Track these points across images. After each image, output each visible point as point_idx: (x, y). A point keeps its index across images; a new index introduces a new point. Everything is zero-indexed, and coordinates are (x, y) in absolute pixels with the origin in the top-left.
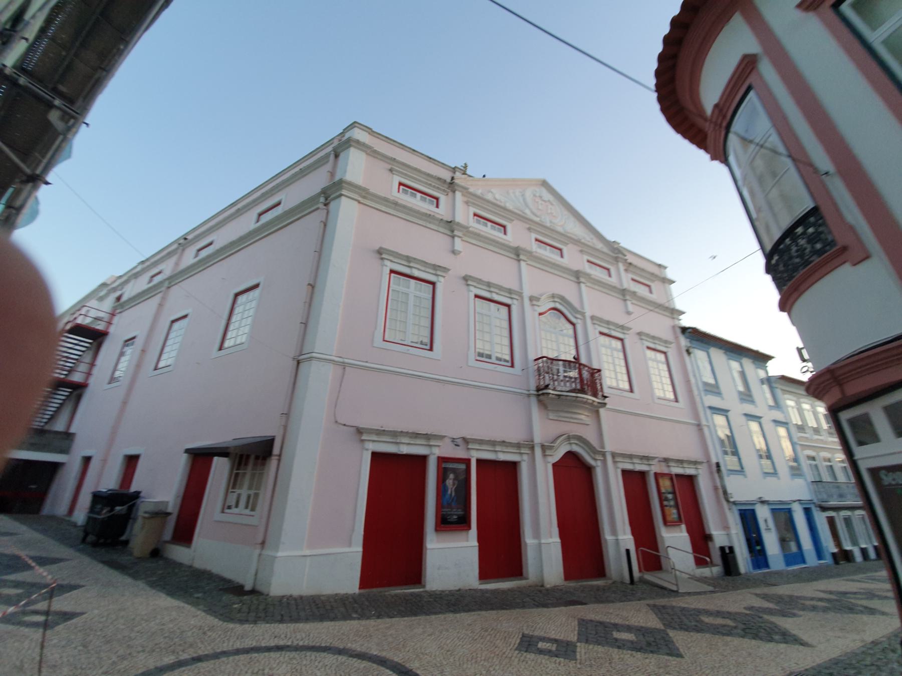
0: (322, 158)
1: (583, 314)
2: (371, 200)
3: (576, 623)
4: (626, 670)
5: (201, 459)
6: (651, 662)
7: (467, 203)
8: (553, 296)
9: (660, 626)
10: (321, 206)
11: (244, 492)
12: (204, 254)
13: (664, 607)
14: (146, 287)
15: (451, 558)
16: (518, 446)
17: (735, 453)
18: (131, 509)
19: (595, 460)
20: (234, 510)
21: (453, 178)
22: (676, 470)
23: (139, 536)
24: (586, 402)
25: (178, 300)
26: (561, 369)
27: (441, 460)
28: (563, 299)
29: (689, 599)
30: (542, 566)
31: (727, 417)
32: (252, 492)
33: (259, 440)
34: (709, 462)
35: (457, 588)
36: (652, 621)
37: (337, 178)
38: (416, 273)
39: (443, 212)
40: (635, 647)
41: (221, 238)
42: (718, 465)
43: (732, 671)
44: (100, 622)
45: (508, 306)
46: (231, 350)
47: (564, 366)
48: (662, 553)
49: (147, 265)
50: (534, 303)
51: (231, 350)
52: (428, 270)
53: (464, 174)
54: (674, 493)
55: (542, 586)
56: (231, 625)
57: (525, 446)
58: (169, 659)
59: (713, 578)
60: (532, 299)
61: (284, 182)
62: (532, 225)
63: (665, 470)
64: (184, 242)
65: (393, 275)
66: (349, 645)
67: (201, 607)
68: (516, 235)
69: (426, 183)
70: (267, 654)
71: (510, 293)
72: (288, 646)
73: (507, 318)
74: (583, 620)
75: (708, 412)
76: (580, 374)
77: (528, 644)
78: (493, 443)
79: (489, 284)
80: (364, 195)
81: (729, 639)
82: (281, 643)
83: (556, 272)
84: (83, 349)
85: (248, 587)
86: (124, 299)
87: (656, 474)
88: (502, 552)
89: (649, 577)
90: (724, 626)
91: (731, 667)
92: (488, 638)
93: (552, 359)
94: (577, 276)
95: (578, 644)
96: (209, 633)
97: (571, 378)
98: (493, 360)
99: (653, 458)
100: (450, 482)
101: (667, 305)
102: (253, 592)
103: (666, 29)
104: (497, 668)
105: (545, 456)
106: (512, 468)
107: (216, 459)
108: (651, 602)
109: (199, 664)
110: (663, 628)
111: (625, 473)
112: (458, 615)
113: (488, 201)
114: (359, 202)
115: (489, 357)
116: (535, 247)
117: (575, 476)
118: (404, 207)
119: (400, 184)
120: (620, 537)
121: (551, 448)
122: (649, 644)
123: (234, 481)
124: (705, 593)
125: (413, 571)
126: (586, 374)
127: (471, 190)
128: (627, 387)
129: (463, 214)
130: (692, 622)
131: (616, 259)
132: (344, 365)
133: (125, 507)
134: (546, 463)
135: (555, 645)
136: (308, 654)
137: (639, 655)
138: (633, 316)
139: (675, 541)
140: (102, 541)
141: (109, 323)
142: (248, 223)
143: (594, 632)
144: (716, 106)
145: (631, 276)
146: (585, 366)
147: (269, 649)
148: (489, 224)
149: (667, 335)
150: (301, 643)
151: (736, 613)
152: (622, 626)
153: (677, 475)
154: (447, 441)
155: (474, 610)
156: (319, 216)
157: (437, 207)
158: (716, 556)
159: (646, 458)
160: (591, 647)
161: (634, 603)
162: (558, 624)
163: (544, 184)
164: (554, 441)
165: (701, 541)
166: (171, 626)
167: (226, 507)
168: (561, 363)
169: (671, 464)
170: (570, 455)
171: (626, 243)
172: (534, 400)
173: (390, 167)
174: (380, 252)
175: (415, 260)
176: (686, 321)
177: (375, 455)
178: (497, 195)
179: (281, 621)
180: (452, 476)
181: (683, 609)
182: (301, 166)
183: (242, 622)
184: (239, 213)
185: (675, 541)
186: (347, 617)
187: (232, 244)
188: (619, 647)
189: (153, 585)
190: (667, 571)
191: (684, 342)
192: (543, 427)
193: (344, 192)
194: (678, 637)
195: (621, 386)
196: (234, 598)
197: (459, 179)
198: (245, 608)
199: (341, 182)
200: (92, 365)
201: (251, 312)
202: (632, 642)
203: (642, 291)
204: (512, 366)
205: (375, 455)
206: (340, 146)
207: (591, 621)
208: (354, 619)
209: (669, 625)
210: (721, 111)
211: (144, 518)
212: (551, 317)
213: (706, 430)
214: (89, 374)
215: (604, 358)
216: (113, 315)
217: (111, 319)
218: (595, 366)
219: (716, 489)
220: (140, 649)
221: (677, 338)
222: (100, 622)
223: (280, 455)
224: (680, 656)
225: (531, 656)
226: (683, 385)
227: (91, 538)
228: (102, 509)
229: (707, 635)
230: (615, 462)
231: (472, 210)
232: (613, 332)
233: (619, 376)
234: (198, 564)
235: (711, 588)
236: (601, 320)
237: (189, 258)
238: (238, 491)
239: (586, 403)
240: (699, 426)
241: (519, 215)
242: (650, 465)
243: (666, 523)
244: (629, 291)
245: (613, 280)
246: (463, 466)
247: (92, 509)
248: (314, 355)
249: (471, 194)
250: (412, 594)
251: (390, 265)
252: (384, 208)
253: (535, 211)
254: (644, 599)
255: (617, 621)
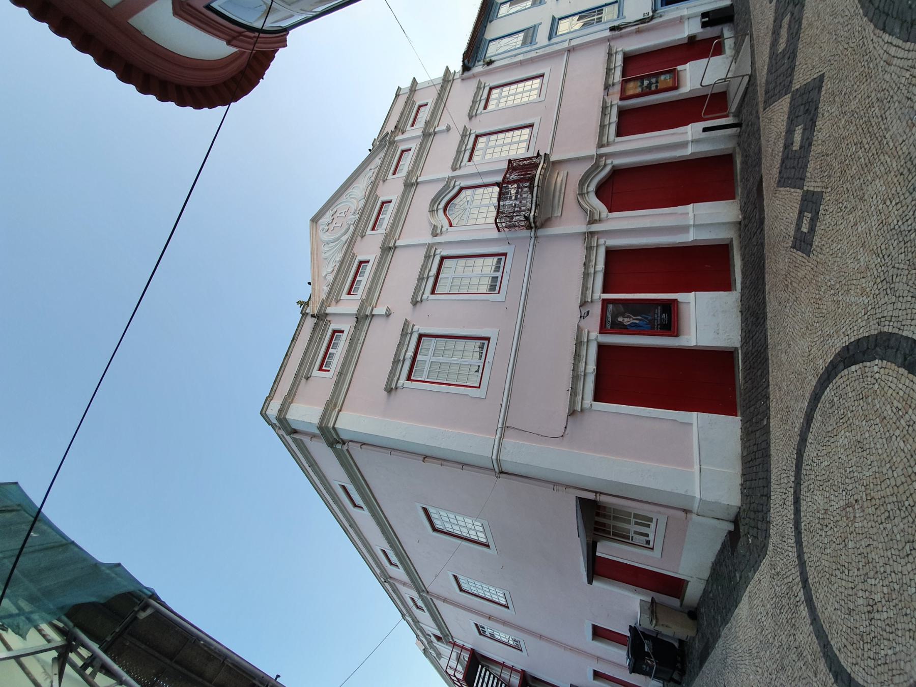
0: (298, 446)
1: (450, 179)
2: (338, 398)
3: (781, 189)
4: (835, 138)
5: (598, 569)
6: (827, 110)
7: (337, 302)
8: (432, 211)
9: (787, 98)
10: (345, 447)
11: (633, 528)
12: (394, 559)
13: (767, 92)
14: (427, 614)
15: (707, 320)
16: (589, 249)
17: (599, 9)
18: (647, 637)
19: (605, 165)
20: (651, 538)
21: (313, 316)
22: (617, 76)
23: (674, 630)
24: (544, 176)
25: (439, 583)
26: (508, 202)
27: (603, 330)
28: (435, 200)
29: (758, 64)
30: (719, 224)
31: (560, 19)
32: (633, 520)
33: (581, 521)
34: (609, 39)
35: (740, 314)
36: (783, 105)
37: (317, 432)
38: (410, 354)
39: (347, 326)
40: (810, 127)
41: (379, 542)
42: (612, 29)
43: (841, 21)
44: (763, 674)
45: (443, 258)
46: (489, 536)
47: (506, 199)
48: (709, 92)
49: (406, 613)
50: (439, 231)
51: (489, 536)
52: (407, 343)
53: (307, 304)
54: (642, 79)
55: (740, 223)
56: (771, 547)
57: (589, 242)
58: (804, 611)
59: (736, 37)
60: (435, 234)
61: (322, 483)
62: (358, 232)
63: (618, 88)
64: (385, 579)
65: (412, 378)
66: (796, 430)
67: (750, 574)
68: (369, 249)
69: (319, 342)
70: (802, 514)
71: (430, 256)
72: (795, 492)
73: (455, 260)
74: (779, 181)
75: (554, 40)
76: (513, 182)
77: (803, 243)
78: (586, 275)
79: (420, 279)
80: (333, 405)
81: (804, 22)
82: (791, 498)
83: (406, 209)
84: (488, 673)
85: (731, 527)
86: (438, 633)
87: (621, 99)
88: (701, 266)
89: (733, 108)
90: (790, 27)
91: (837, 21)
92: (795, 285)
93: (498, 212)
94: (410, 185)
95: (805, 188)
96: (778, 569)
97: (517, 193)
98: (499, 274)
99: (604, 102)
100: (627, 321)
101: (439, 87)
102: (736, 522)
103: (152, 98)
104: (828, 278)
105: (600, 221)
106: (611, 254)
107: (597, 554)
108: (761, 106)
109: (810, 581)
110: (790, 95)
111: (618, 134)
112: (769, 315)
113: (335, 279)
114: (340, 410)
115: (494, 279)
116: (382, 230)
117: (623, 187)
118: (343, 365)
119: (320, 369)
120: (690, 139)
121: (592, 214)
122: (807, 111)
123: (623, 537)
124: (752, 46)
125: (719, 359)
126: (514, 176)
127: (324, 296)
128: (527, 131)
129: (349, 305)
130: (784, 62)
131: (392, 143)
132: (505, 428)
133: (645, 642)
134: (607, 219)
135: (806, 214)
136: (804, 472)
137: (819, 123)
138: (452, 126)
139: (694, 76)
140: (678, 665)
141: (463, 648)
142: (363, 517)
143: (793, 170)
144: (229, 43)
145: (409, 128)
146: (505, 177)
147: (797, 511)
148: (358, 278)
149: (472, 85)
150: (793, 479)
151: (776, 12)
152: (786, 139)
153: (623, 75)
154: (583, 323)
155: (764, 298)
156: (355, 449)
157: (342, 332)
158: (711, 32)
159: (604, 109)
160: (808, 175)
161: (762, 125)
162: (782, 209)
163: (315, 220)
164: (585, 210)
165: (695, 49)
166: (769, 606)
167: (648, 546)
168: (502, 203)
169: (611, 82)
170: (599, 193)
171: (373, 132)
172: (541, 232)
173: (304, 380)
174: (389, 390)
175: (397, 354)
176: (456, 66)
177: (596, 399)
178: (328, 270)
179: (768, 497)
180: (620, 319)
181: (769, 71)
182: (307, 466)
183: (767, 536)
184: (353, 525)
185: (694, 76)
186: (767, 431)
187: (384, 532)
188: (810, 144)
189: (725, 621)
190: (728, 86)
191: (478, 68)
192: (570, 223)
193: (331, 425)
194: (801, 79)
195: (526, 137)
196: (742, 540)
197: (313, 309)
198: (754, 532)
199: (320, 428)
200: (503, 665)
201: (452, 516)
202: (804, 130)
203: (424, 114)
204: (505, 255)
205: (596, 399)
206: (285, 427)
207: (780, 173)
208: (768, 423)
209: (787, 89)
210: (234, 38)
211: (656, 625)
212: (454, 214)
213: (574, 43)
214: (512, 669)
215: (496, 156)
216: (455, 644)
217: (458, 646)
218: (505, 165)
219: (638, 32)
220: (792, 638)
221: (474, 76)
222: (763, 674)
223: (596, 492)
224: (821, 78)
225: (816, 241)
226: (527, 68)
227: (676, 676)
228: (647, 664)
229: (800, 46)
230: (608, 144)
231: (344, 296)
232: (469, 144)
233: (516, 139)
234: (706, 574)
235: (747, 38)
236: (456, 160)
237: (399, 573)
238: (632, 534)
239: (544, 176)
240: (570, 50)
241: (348, 247)
242: (611, 106)
243: (675, 88)
244: (425, 129)
245: (414, 145)
246: (610, 307)
247: (647, 674)
248: (494, 457)
249: (328, 297)
250: (744, 362)
251: (402, 381)
252: (345, 386)
253: (343, 231)
254: (757, 112)
255: (781, 144)
